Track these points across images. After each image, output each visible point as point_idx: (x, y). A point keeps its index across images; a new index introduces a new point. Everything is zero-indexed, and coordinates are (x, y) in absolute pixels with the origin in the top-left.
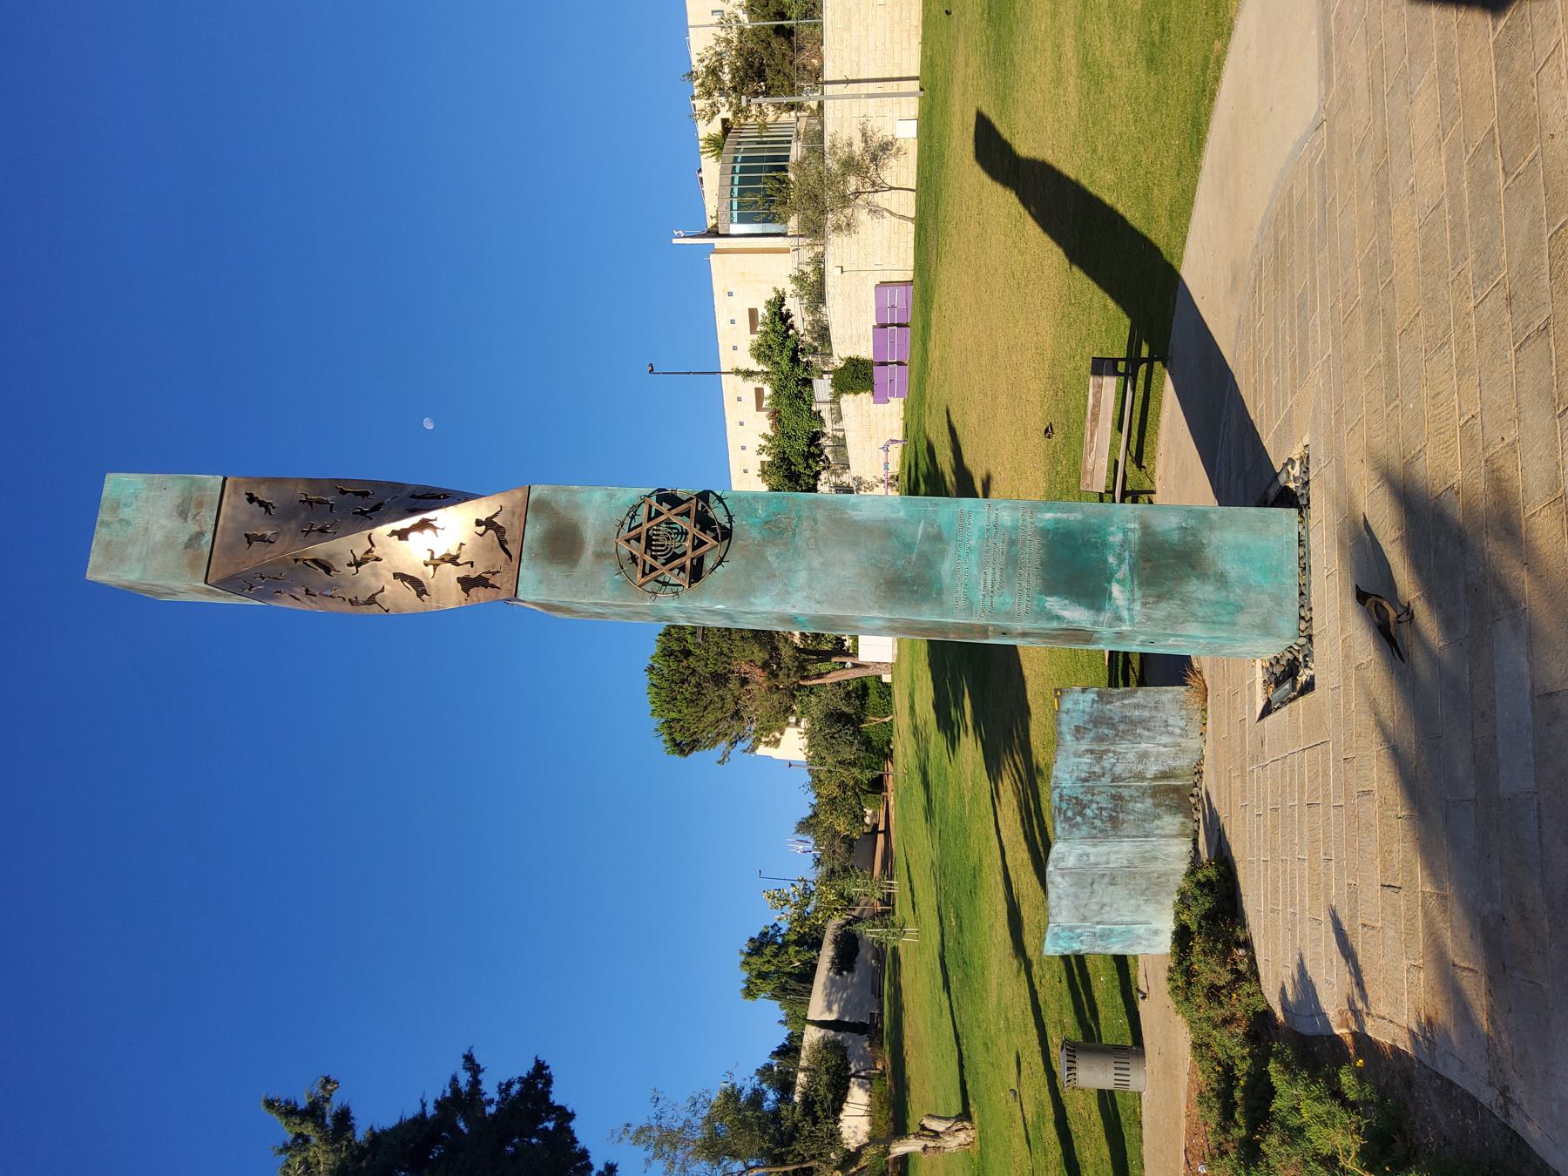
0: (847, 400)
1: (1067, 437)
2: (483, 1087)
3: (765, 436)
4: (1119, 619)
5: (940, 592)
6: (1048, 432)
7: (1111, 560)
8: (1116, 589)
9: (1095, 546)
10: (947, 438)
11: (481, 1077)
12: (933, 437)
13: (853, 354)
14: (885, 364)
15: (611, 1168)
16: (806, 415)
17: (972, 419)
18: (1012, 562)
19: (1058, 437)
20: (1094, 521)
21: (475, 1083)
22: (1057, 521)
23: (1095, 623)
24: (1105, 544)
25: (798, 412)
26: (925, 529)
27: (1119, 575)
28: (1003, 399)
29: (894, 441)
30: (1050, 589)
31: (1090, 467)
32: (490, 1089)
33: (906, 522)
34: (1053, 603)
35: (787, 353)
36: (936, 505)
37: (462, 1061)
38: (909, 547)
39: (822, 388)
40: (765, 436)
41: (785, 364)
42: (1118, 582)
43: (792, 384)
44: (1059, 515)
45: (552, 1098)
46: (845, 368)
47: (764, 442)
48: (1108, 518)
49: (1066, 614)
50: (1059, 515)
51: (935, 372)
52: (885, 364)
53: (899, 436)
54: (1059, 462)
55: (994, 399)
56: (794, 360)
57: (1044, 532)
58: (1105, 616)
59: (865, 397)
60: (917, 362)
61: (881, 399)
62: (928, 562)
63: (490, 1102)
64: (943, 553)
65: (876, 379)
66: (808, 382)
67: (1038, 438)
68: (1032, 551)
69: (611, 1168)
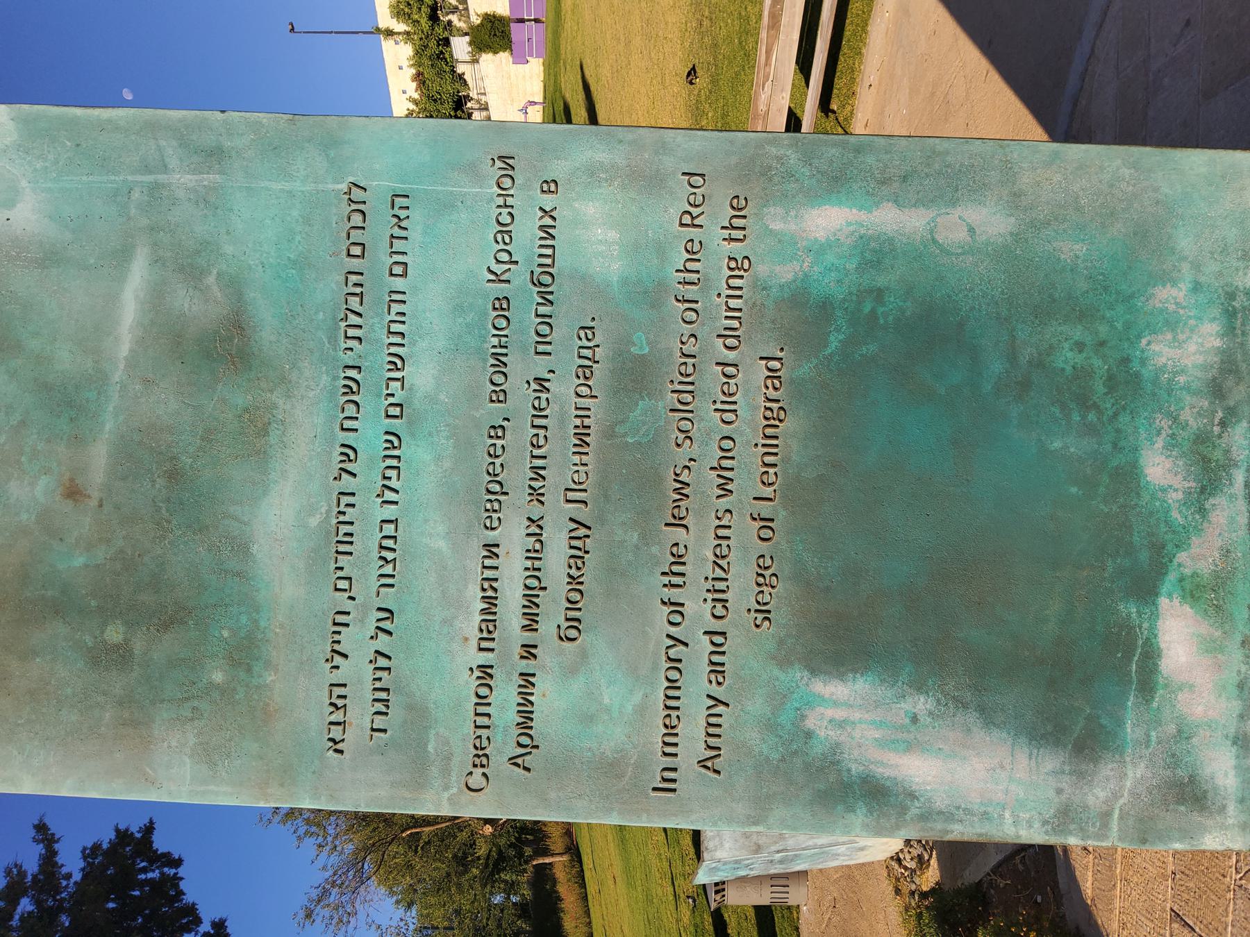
0: (486, 58)
1: (714, 81)
2: (60, 859)
3: (411, 100)
4: (1189, 793)
5: (245, 653)
6: (692, 72)
7: (1160, 470)
8: (1178, 634)
9: (1076, 393)
10: (581, 96)
11: (56, 846)
12: (569, 99)
13: (489, 10)
14: (522, 21)
15: (219, 926)
16: (448, 76)
17: (605, 71)
18: (642, 487)
19: (702, 81)
20: (1071, 249)
21: (49, 859)
22: (875, 252)
23: (1065, 816)
24: (1128, 384)
25: (440, 74)
26: (156, 297)
27: (1197, 558)
28: (637, 41)
29: (533, 103)
30: (839, 640)
31: (762, 107)
32: (72, 863)
33: (49, 258)
34: (850, 711)
35: (425, 10)
36: (215, 156)
37: (33, 833)
38: (67, 402)
39: (460, 47)
40: (411, 100)
41: (425, 23)
42: (1193, 591)
43: (433, 43)
44: (890, 219)
45: (155, 846)
46: (482, 24)
47: (412, 107)
48: (1148, 240)
49: (921, 771)
50: (890, 219)
51: (569, 24)
52: (522, 21)
53: (539, 98)
54: (704, 113)
55: (628, 43)
56: (434, 18)
57: (805, 315)
58: (1122, 782)
59: (504, 56)
60: (551, 15)
61: (520, 59)
62: (178, 490)
63: (68, 876)
64: (256, 434)
65: (514, 37)
66: (447, 42)
67: (677, 86)
68: (737, 417)
69: (219, 926)
